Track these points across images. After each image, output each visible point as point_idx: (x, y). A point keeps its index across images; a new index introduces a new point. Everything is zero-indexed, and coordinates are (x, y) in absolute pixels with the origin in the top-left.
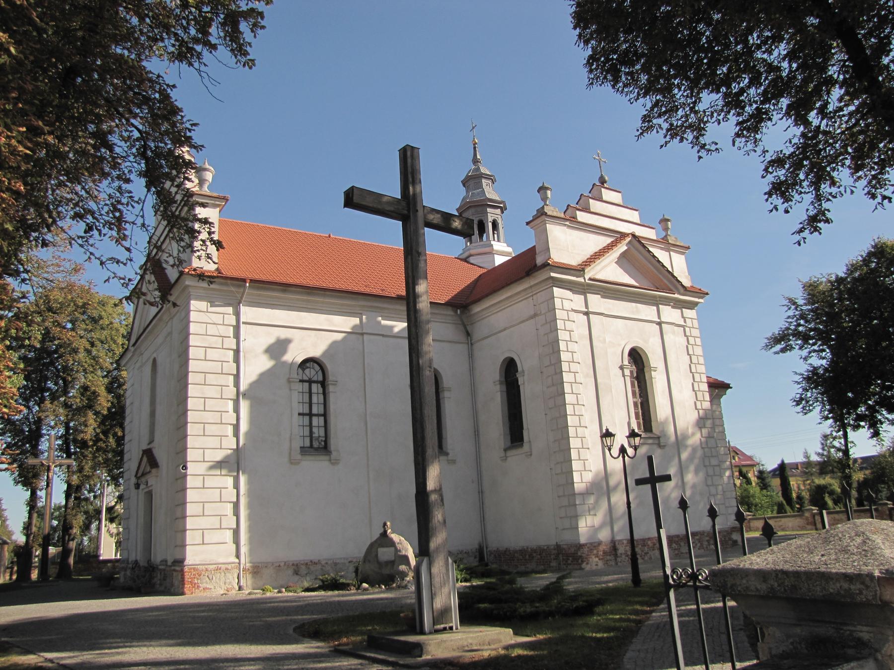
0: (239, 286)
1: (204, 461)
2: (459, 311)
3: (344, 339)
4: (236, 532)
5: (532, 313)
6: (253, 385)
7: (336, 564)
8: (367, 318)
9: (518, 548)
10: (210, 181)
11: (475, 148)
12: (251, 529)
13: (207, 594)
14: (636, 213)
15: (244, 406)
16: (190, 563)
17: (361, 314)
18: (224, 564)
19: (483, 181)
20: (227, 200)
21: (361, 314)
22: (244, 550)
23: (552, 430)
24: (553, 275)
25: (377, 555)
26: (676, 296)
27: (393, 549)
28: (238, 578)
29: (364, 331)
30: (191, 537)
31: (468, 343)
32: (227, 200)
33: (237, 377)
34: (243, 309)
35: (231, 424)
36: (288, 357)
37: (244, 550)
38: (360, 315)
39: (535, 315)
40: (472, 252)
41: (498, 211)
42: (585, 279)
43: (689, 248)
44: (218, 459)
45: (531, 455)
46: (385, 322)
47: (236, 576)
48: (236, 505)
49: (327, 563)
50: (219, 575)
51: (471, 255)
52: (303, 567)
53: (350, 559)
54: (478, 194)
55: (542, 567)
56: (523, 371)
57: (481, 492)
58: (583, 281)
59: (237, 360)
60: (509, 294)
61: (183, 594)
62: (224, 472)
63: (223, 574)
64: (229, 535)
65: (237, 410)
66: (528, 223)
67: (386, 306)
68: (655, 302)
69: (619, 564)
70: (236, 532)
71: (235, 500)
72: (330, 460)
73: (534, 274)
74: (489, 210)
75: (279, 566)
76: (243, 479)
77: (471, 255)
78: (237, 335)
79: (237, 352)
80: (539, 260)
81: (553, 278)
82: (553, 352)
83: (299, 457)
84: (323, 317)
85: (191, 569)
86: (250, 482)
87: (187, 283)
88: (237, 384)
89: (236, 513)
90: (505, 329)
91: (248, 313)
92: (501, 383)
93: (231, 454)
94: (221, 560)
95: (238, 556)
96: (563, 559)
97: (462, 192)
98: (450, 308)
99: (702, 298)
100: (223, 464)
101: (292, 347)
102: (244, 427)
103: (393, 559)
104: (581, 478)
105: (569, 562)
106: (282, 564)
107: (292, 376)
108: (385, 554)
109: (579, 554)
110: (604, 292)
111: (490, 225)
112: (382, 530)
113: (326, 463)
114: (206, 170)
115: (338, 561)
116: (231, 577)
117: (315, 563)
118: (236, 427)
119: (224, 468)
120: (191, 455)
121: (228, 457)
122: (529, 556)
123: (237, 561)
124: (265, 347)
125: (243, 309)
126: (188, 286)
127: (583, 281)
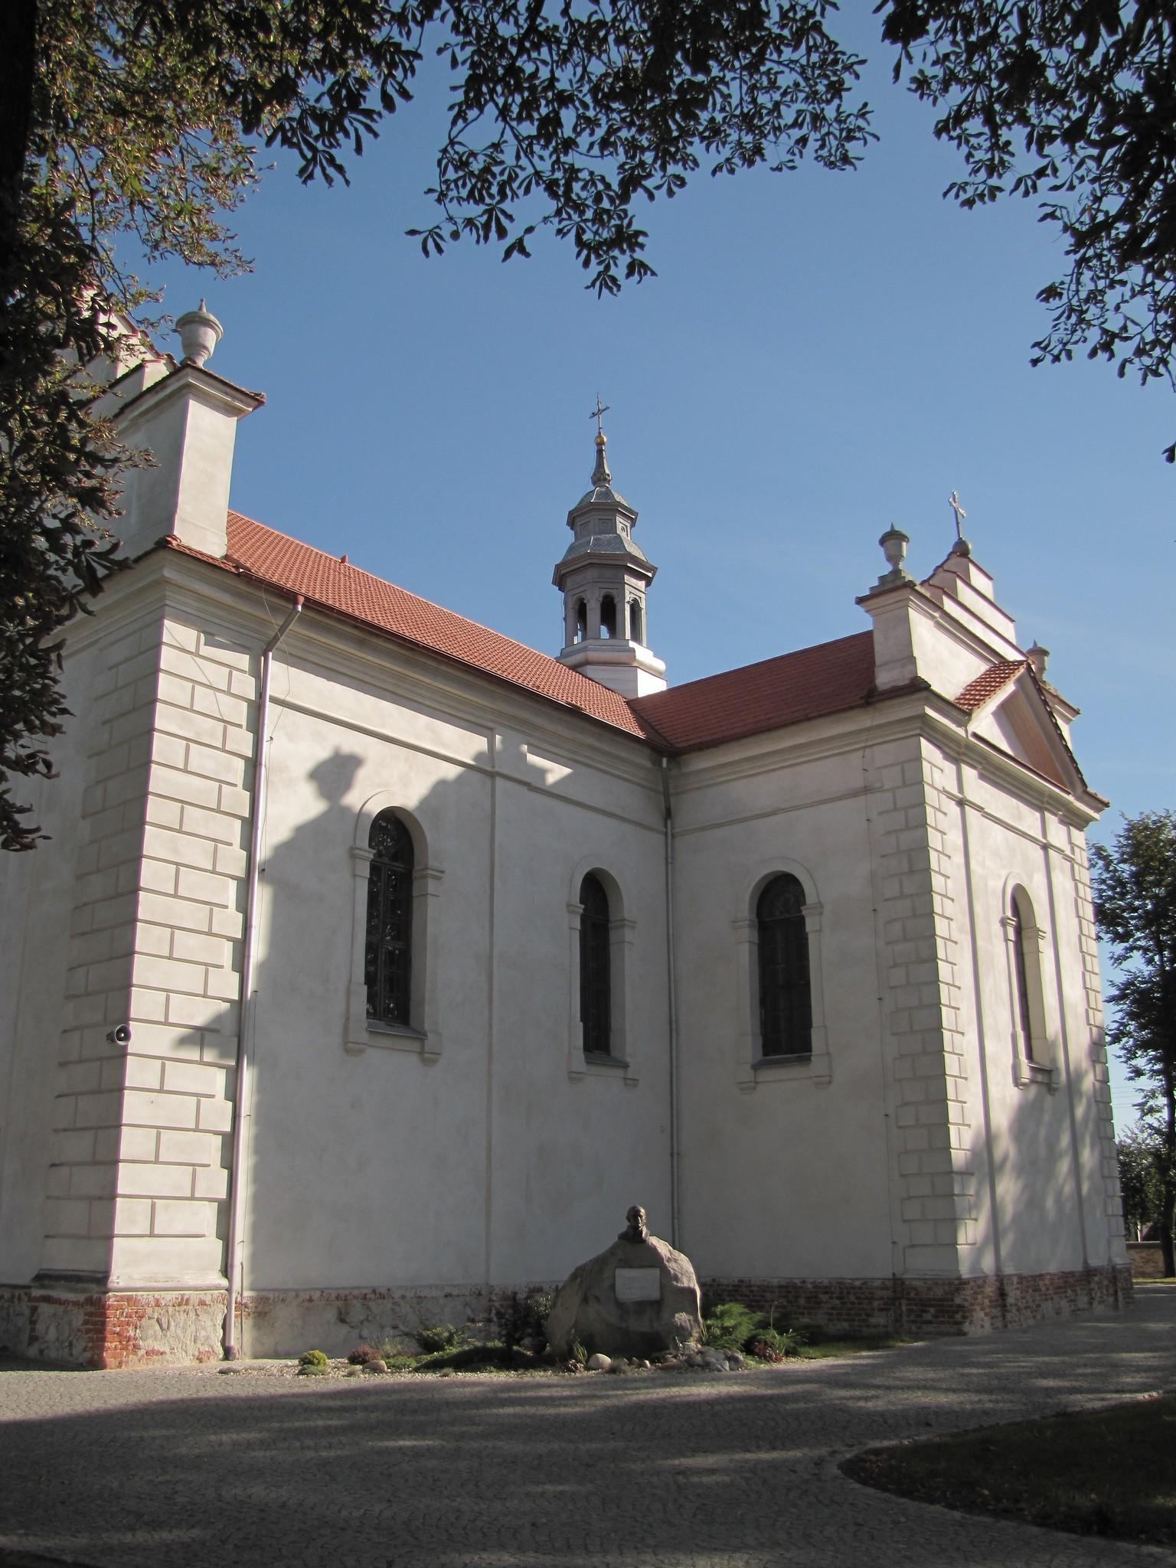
0: (275, 609)
1: (166, 1023)
2: (665, 761)
3: (460, 779)
4: (226, 1209)
5: (858, 782)
6: (283, 850)
7: (420, 1299)
8: (503, 742)
9: (775, 1282)
10: (212, 350)
11: (600, 452)
12: (258, 1202)
13: (155, 1365)
14: (1011, 625)
15: (262, 897)
16: (122, 1284)
17: (491, 729)
18: (196, 1289)
19: (619, 519)
20: (261, 403)
21: (491, 729)
22: (241, 1254)
23: (894, 1034)
24: (929, 712)
25: (613, 1287)
26: (1071, 798)
27: (657, 1271)
28: (224, 1327)
29: (497, 769)
30: (127, 1216)
31: (666, 834)
32: (261, 403)
33: (250, 825)
34: (276, 669)
35: (229, 939)
36: (353, 799)
37: (241, 1254)
38: (489, 732)
39: (866, 790)
40: (593, 655)
41: (641, 584)
42: (966, 731)
43: (1077, 712)
44: (199, 1020)
45: (830, 1082)
46: (534, 759)
47: (220, 1322)
48: (230, 1141)
49: (403, 1297)
50: (183, 1316)
51: (587, 663)
52: (357, 1304)
53: (448, 1290)
54: (609, 542)
55: (846, 1325)
56: (820, 905)
57: (675, 1155)
58: (964, 735)
59: (252, 783)
60: (802, 740)
61: (95, 1363)
62: (209, 1056)
63: (192, 1314)
64: (208, 1215)
65: (244, 906)
66: (860, 601)
67: (539, 721)
68: (1040, 802)
69: (1009, 1325)
70: (226, 1209)
71: (227, 1128)
72: (421, 1053)
73: (879, 705)
74: (627, 578)
75: (311, 1300)
76: (248, 1076)
77: (587, 663)
78: (256, 725)
79: (254, 765)
80: (884, 679)
81: (924, 717)
82: (911, 872)
83: (364, 1037)
84: (423, 720)
85: (122, 1298)
86: (261, 1088)
87: (167, 573)
88: (249, 842)
89: (229, 1163)
90: (774, 813)
91: (282, 677)
92: (751, 926)
93: (227, 1013)
94: (191, 1280)
95: (226, 1271)
96: (910, 1311)
97: (569, 536)
98: (648, 751)
99: (1098, 810)
100: (208, 1036)
101: (362, 775)
102: (257, 951)
103: (655, 1295)
104: (962, 1140)
105: (928, 1317)
106: (316, 1295)
107: (359, 844)
108: (633, 1284)
109: (958, 1301)
110: (984, 768)
111: (627, 608)
112: (624, 1226)
113: (414, 1059)
114: (207, 323)
115: (425, 1293)
116: (209, 1323)
117: (382, 1297)
118: (242, 948)
119: (212, 1045)
120: (142, 1004)
121: (219, 1018)
122: (808, 1299)
123: (225, 1282)
124: (309, 765)
125: (276, 669)
126: (165, 582)
127: (964, 735)
